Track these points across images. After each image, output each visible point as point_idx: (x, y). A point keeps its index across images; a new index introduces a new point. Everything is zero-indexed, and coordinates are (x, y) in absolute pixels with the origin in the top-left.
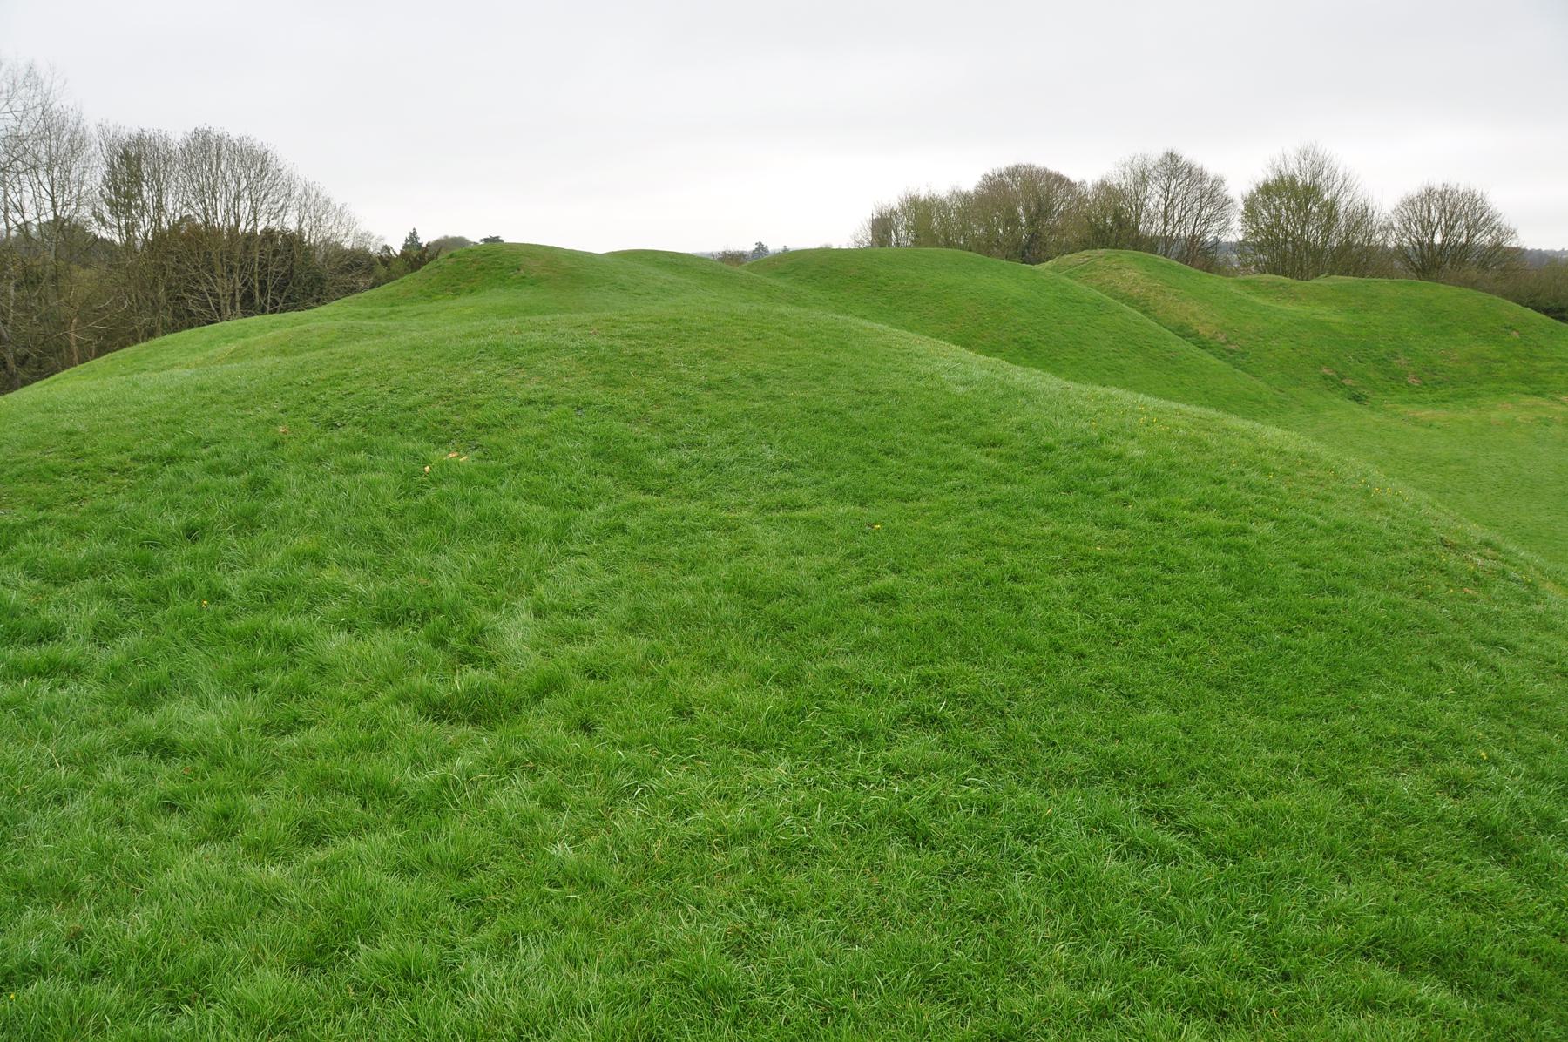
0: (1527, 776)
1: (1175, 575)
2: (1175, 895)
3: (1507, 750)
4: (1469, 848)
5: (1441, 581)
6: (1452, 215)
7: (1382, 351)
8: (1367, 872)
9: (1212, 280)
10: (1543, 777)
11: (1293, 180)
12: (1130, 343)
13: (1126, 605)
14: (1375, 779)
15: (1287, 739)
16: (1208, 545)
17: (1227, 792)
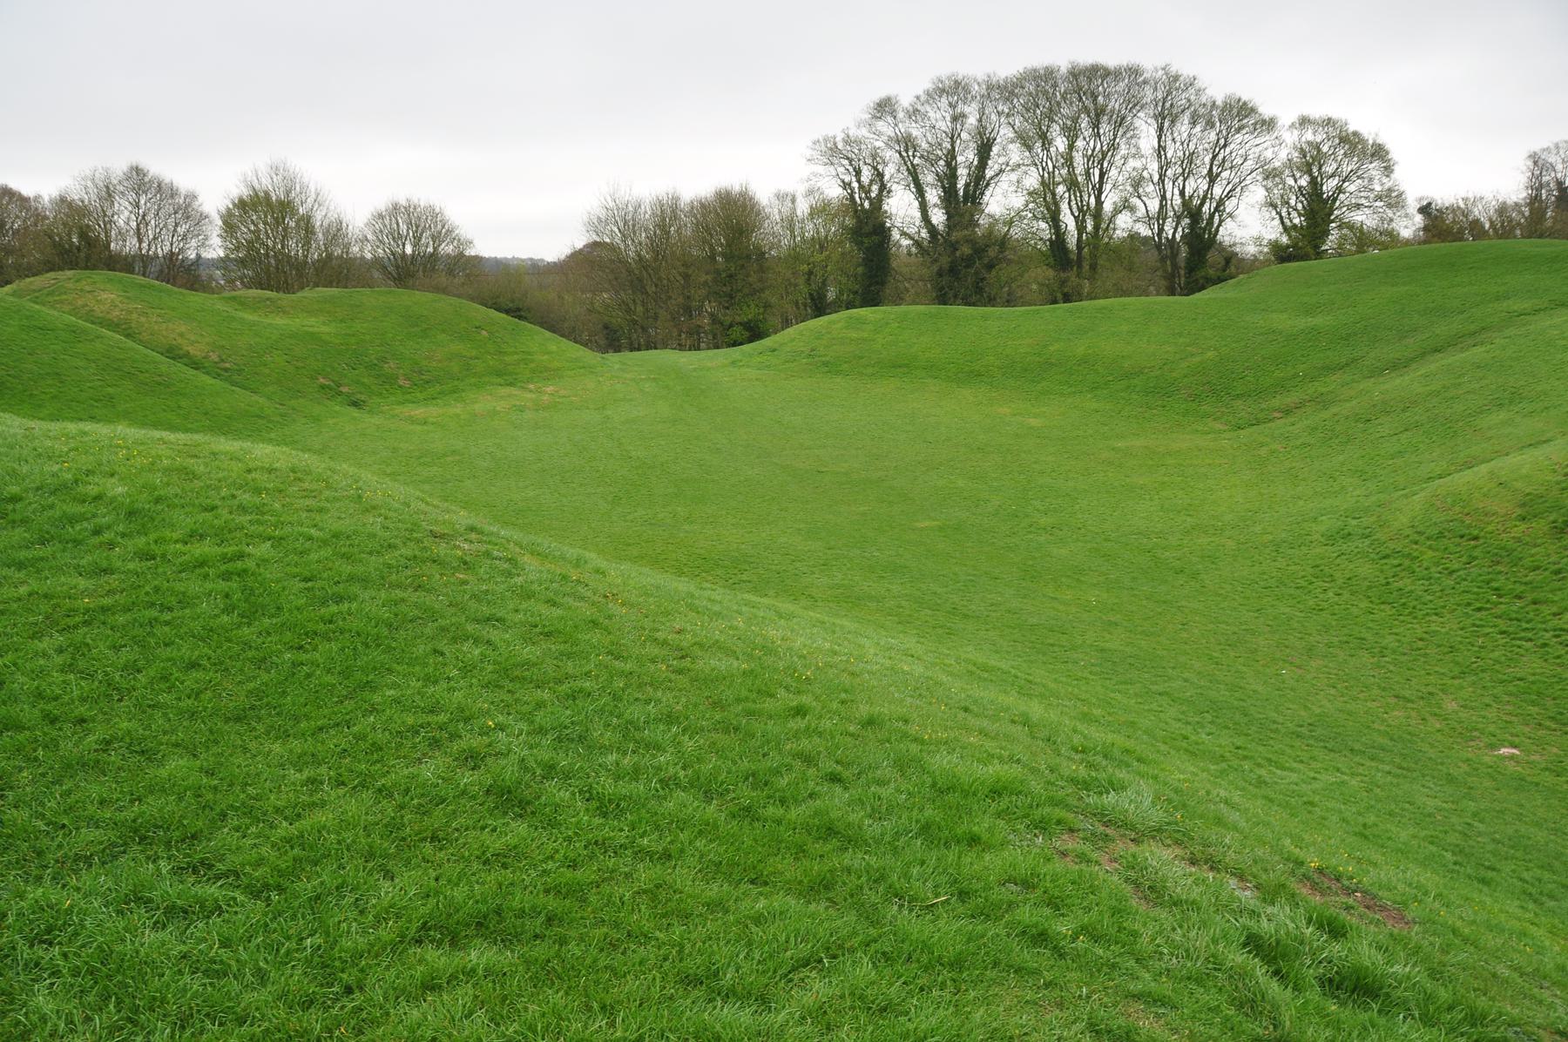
0: (529, 733)
1: (176, 613)
2: (224, 947)
3: (509, 714)
4: (491, 812)
5: (434, 570)
6: (417, 227)
7: (373, 357)
8: (408, 862)
9: (196, 299)
10: (542, 731)
11: (267, 193)
12: (116, 369)
13: (126, 655)
14: (401, 772)
15: (313, 755)
16: (206, 576)
17: (261, 825)
